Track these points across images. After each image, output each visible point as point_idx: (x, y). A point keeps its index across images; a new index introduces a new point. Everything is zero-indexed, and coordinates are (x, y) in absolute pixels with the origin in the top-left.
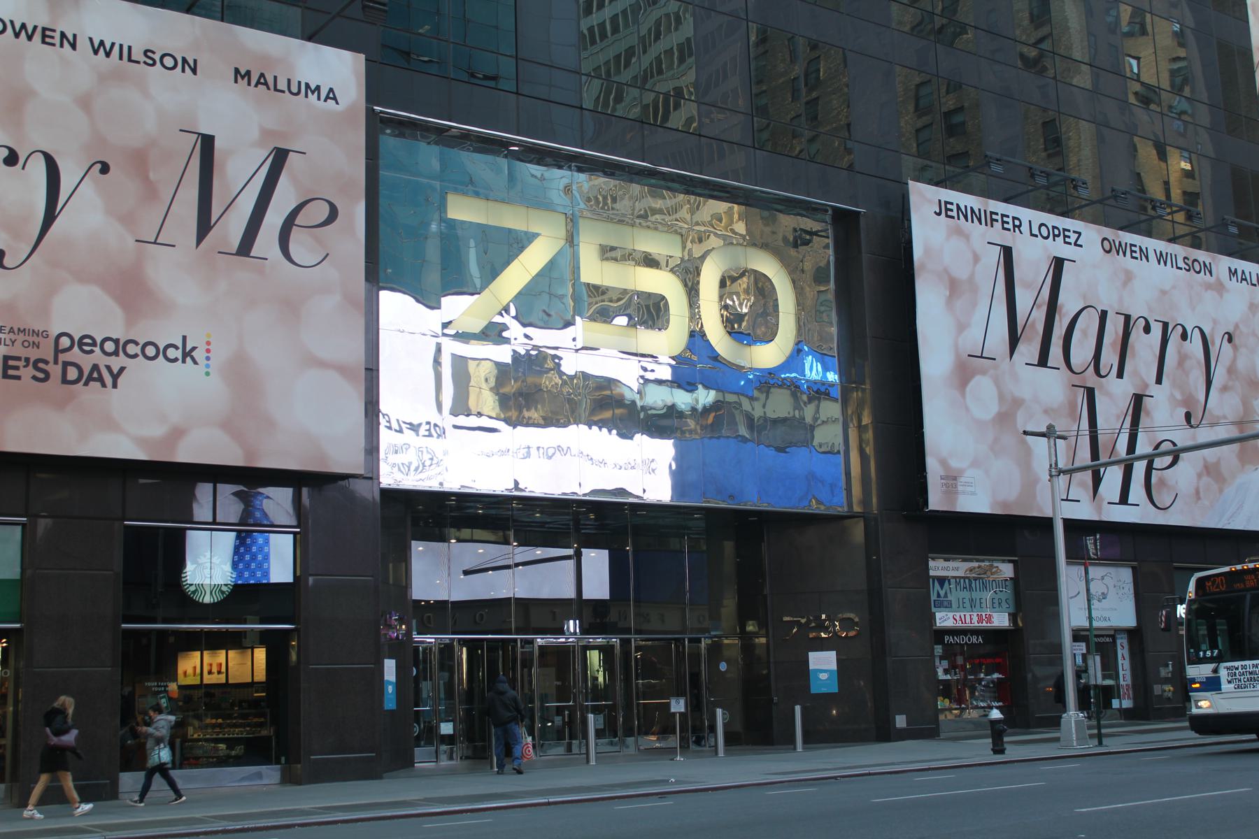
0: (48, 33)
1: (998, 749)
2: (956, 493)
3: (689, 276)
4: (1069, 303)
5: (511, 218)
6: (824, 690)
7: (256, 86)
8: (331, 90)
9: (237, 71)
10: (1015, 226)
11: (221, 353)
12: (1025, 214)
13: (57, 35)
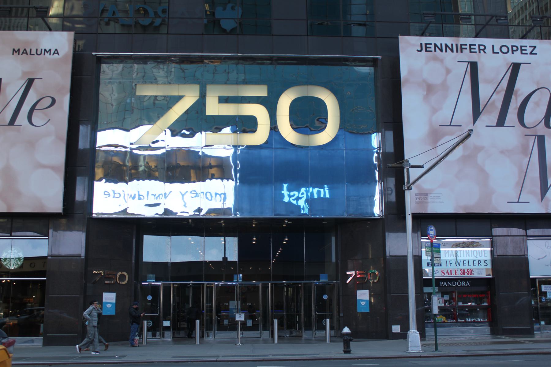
2: (427, 203)
3: (271, 104)
4: (523, 86)
5: (173, 91)
6: (109, 313)
8: (56, 50)
9: (14, 50)
10: (480, 50)
12: (488, 42)
13: (433, 46)
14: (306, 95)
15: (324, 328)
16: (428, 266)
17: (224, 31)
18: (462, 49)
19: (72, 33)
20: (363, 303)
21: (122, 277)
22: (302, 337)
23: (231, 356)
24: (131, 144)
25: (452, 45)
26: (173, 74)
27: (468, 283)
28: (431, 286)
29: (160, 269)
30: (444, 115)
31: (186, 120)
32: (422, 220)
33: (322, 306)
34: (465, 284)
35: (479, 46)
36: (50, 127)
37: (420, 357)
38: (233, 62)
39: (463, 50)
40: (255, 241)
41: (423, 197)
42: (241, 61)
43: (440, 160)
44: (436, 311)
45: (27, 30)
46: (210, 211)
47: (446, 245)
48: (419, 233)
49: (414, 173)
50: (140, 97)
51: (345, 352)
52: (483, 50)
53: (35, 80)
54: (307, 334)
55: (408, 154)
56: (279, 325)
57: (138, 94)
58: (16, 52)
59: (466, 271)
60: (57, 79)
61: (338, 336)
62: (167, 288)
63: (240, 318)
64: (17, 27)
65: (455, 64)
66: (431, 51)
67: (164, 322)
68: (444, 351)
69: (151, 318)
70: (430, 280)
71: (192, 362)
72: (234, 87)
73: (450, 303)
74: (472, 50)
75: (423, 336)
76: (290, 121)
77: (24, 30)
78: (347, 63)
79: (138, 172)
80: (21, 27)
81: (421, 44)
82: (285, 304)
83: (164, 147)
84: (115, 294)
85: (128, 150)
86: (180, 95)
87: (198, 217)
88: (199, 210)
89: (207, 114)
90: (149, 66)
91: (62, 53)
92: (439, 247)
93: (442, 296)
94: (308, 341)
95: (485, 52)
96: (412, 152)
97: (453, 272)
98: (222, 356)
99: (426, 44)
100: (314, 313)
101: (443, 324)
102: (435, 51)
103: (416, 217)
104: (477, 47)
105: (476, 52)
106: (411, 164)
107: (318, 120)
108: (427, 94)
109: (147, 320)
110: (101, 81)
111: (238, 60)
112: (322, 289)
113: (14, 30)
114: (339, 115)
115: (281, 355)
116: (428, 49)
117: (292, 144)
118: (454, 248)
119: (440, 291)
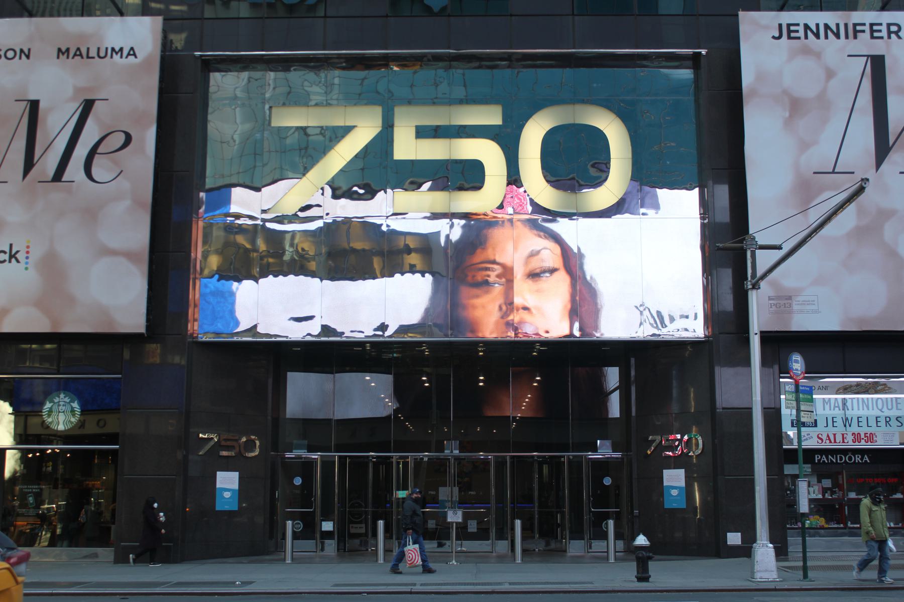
0: (875, 28)
1: (643, 576)
2: (791, 312)
3: (508, 139)
6: (227, 508)
7: (73, 58)
8: (132, 49)
9: (59, 50)
10: (890, 33)
11: (37, 253)
13: (801, 29)
14: (571, 122)
15: (604, 536)
16: (792, 426)
17: (428, 10)
18: (856, 33)
19: (159, 19)
20: (674, 492)
21: (250, 445)
22: (565, 551)
23: (473, 584)
24: (264, 211)
25: (838, 25)
26: (336, 87)
27: (866, 458)
28: (795, 462)
29: (315, 430)
30: (823, 153)
31: (363, 169)
32: (779, 344)
33: (602, 496)
34: (862, 459)
35: (889, 25)
36: (123, 184)
37: (775, 590)
38: (441, 64)
39: (859, 34)
40: (537, 381)
41: (782, 302)
42: (454, 63)
43: (810, 236)
44: (804, 507)
45: (82, 15)
46: (403, 329)
47: (825, 389)
48: (776, 367)
49: (764, 260)
50: (280, 129)
51: (640, 579)
52: (897, 33)
53: (97, 102)
54: (575, 547)
55: (753, 227)
56: (524, 529)
57: (275, 123)
58: (63, 54)
59: (863, 436)
60: (133, 99)
61: (632, 551)
62: (327, 465)
63: (455, 517)
64: (65, 10)
65: (845, 61)
66: (799, 38)
67: (324, 523)
68: (818, 578)
69: (303, 517)
70: (795, 451)
71: (368, 593)
72: (443, 109)
73: (833, 493)
74: (876, 34)
75: (781, 552)
76: (543, 168)
77: (77, 15)
78: (645, 63)
79: (282, 263)
80: (71, 10)
81: (780, 26)
82: (536, 494)
83: (321, 217)
84: (237, 473)
85: (259, 222)
86: (348, 124)
87: (381, 339)
88: (383, 327)
89: (395, 158)
90: (296, 76)
91: (141, 55)
92: (810, 391)
93: (819, 481)
94: (577, 560)
95: (899, 38)
96: (767, 219)
97: (839, 438)
98: (422, 585)
99: (789, 25)
100: (589, 510)
101: (816, 531)
102: (806, 37)
103: (767, 338)
104: (884, 28)
105: (882, 38)
106: (759, 243)
107: (593, 166)
108: (790, 116)
109: (293, 520)
110: (210, 103)
111: (450, 61)
112: (602, 467)
113: (59, 15)
114: (630, 156)
115: (576, 583)
116: (793, 35)
117: (545, 208)
118: (840, 394)
119: (814, 471)
